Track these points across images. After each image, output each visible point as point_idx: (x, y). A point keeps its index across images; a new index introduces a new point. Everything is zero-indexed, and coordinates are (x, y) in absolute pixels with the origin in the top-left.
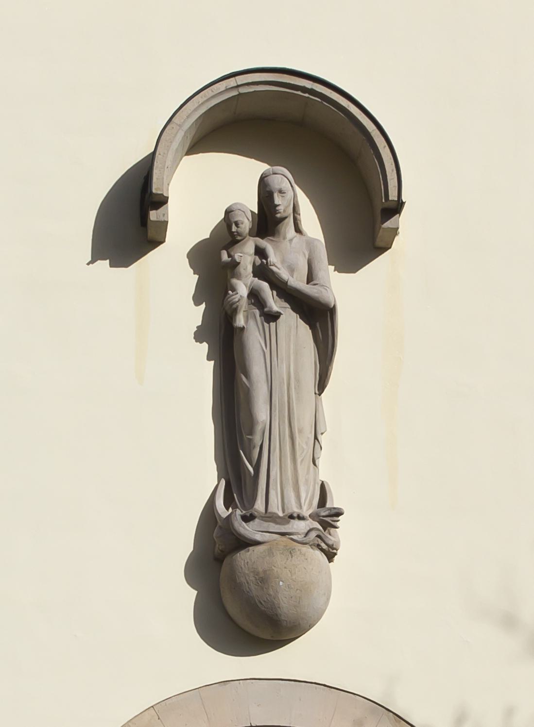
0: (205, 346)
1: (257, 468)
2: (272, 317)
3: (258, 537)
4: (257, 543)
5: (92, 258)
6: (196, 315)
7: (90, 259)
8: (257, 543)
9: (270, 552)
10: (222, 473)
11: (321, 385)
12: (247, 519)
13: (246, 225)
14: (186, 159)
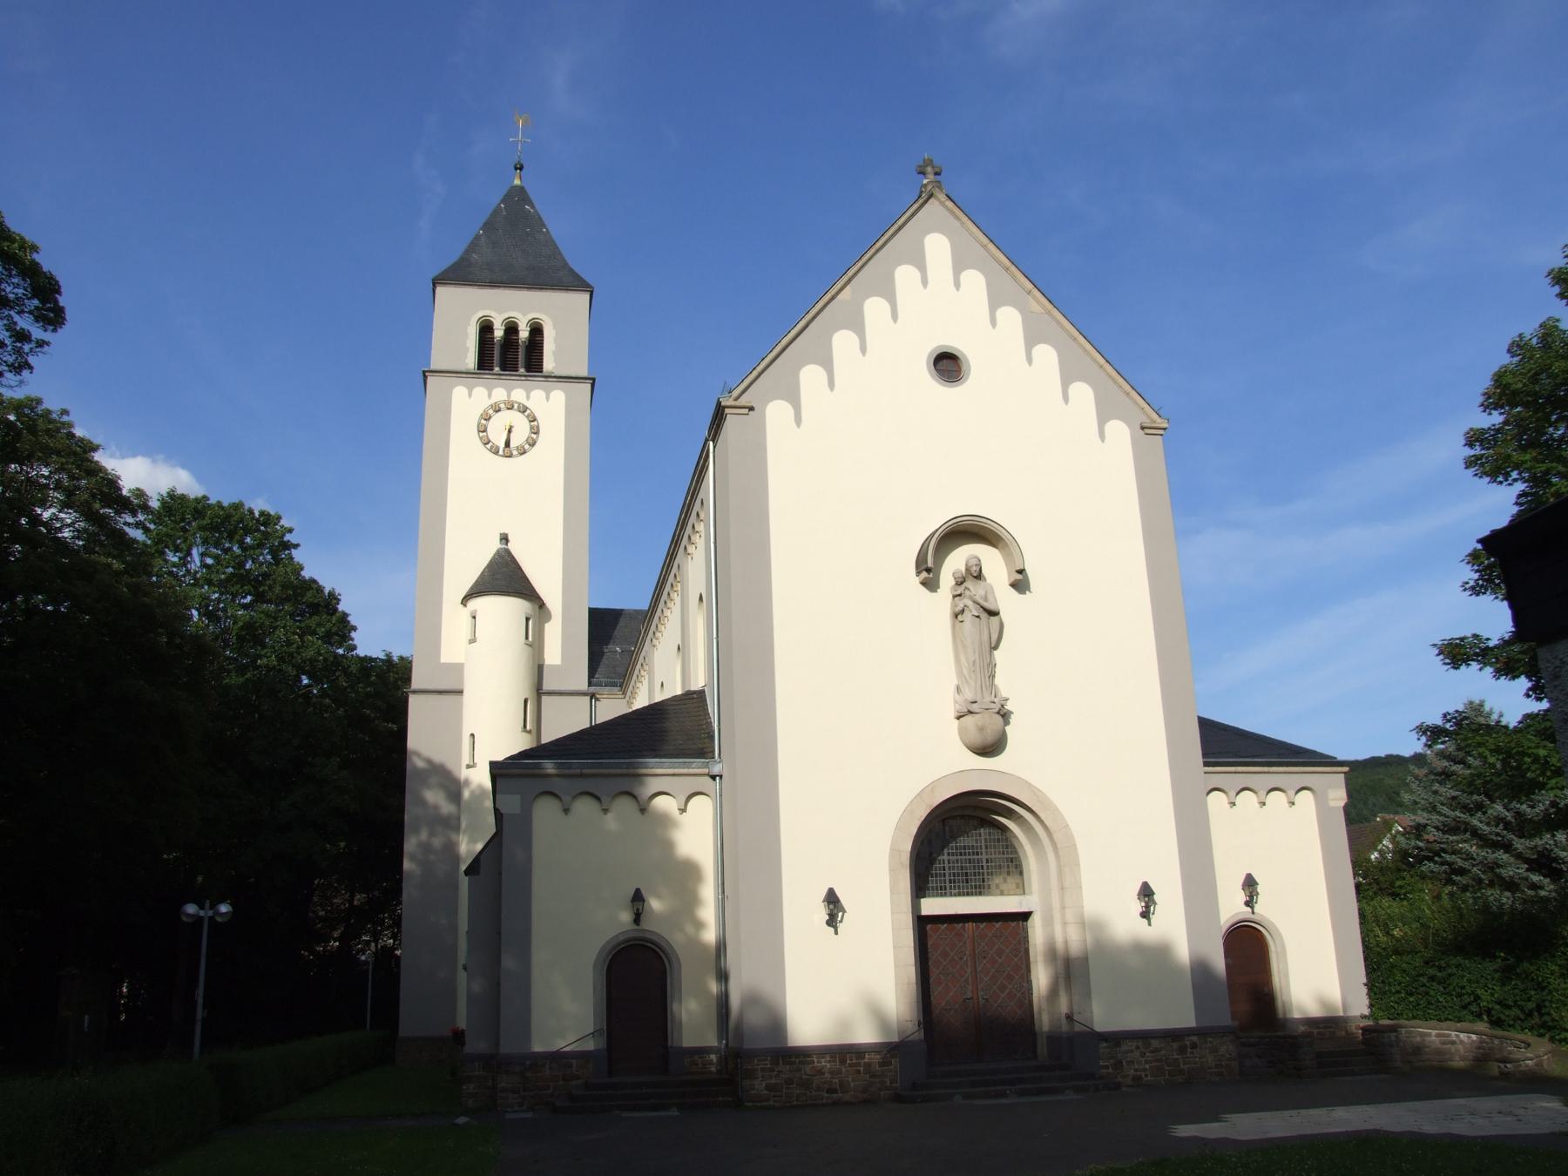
3: (978, 711)
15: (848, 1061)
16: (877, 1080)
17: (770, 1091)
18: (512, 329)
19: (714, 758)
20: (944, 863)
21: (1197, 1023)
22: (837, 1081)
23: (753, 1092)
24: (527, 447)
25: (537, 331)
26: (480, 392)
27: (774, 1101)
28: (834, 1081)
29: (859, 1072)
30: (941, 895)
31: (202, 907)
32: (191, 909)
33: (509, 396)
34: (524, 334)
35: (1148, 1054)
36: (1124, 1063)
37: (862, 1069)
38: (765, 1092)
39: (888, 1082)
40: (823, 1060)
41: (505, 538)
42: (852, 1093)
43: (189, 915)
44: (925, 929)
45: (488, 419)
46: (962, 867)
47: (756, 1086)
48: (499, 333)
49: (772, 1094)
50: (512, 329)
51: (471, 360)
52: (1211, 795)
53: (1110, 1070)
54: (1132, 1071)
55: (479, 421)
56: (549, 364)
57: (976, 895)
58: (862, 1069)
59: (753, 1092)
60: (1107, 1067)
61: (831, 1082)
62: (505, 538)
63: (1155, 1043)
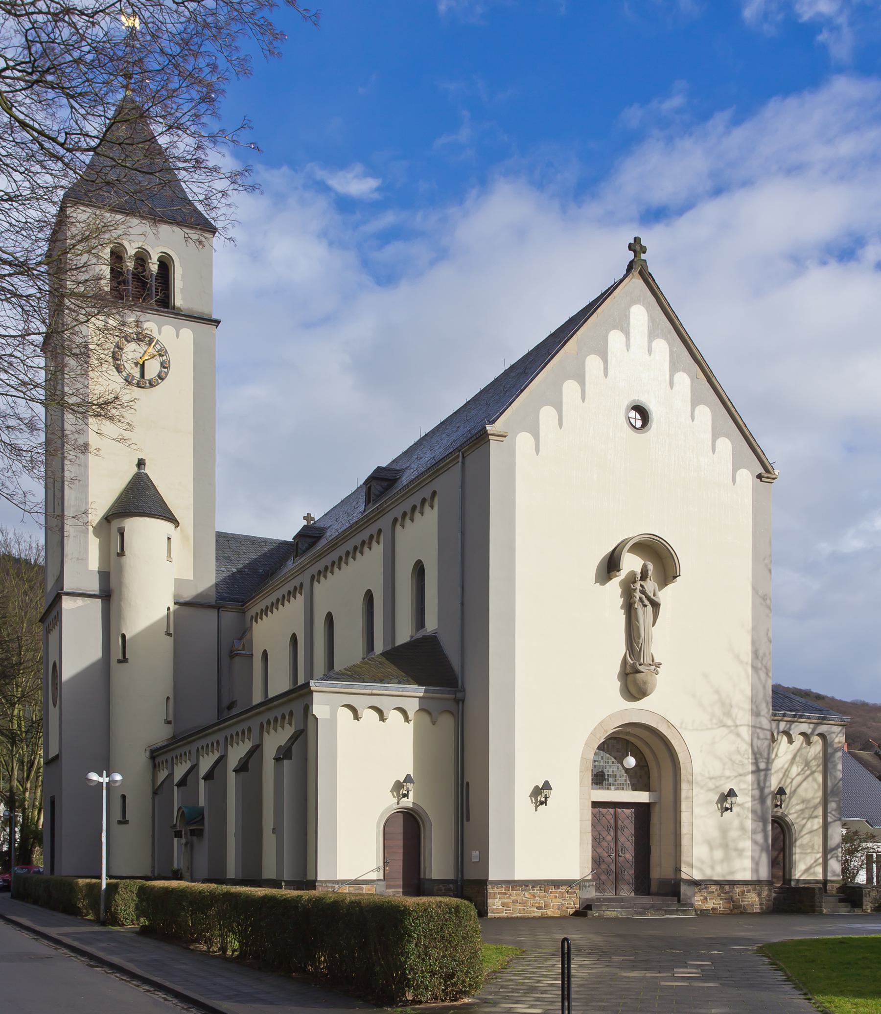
0: (623, 611)
1: (640, 649)
2: (645, 606)
3: (643, 671)
4: (643, 672)
5: (584, 362)
6: (621, 601)
7: (148, 470)
8: (643, 672)
9: (647, 675)
10: (627, 649)
11: (653, 626)
12: (640, 665)
13: (639, 576)
14: (57, 753)
15: (550, 890)
18: (142, 258)
19: (458, 687)
20: (603, 768)
22: (543, 902)
25: (165, 265)
29: (556, 897)
30: (600, 789)
31: (101, 776)
32: (94, 776)
34: (154, 268)
38: (501, 907)
41: (141, 463)
49: (505, 908)
50: (142, 258)
52: (346, 709)
53: (700, 903)
56: (179, 301)
57: (620, 789)
58: (558, 895)
62: (141, 463)
63: (727, 888)
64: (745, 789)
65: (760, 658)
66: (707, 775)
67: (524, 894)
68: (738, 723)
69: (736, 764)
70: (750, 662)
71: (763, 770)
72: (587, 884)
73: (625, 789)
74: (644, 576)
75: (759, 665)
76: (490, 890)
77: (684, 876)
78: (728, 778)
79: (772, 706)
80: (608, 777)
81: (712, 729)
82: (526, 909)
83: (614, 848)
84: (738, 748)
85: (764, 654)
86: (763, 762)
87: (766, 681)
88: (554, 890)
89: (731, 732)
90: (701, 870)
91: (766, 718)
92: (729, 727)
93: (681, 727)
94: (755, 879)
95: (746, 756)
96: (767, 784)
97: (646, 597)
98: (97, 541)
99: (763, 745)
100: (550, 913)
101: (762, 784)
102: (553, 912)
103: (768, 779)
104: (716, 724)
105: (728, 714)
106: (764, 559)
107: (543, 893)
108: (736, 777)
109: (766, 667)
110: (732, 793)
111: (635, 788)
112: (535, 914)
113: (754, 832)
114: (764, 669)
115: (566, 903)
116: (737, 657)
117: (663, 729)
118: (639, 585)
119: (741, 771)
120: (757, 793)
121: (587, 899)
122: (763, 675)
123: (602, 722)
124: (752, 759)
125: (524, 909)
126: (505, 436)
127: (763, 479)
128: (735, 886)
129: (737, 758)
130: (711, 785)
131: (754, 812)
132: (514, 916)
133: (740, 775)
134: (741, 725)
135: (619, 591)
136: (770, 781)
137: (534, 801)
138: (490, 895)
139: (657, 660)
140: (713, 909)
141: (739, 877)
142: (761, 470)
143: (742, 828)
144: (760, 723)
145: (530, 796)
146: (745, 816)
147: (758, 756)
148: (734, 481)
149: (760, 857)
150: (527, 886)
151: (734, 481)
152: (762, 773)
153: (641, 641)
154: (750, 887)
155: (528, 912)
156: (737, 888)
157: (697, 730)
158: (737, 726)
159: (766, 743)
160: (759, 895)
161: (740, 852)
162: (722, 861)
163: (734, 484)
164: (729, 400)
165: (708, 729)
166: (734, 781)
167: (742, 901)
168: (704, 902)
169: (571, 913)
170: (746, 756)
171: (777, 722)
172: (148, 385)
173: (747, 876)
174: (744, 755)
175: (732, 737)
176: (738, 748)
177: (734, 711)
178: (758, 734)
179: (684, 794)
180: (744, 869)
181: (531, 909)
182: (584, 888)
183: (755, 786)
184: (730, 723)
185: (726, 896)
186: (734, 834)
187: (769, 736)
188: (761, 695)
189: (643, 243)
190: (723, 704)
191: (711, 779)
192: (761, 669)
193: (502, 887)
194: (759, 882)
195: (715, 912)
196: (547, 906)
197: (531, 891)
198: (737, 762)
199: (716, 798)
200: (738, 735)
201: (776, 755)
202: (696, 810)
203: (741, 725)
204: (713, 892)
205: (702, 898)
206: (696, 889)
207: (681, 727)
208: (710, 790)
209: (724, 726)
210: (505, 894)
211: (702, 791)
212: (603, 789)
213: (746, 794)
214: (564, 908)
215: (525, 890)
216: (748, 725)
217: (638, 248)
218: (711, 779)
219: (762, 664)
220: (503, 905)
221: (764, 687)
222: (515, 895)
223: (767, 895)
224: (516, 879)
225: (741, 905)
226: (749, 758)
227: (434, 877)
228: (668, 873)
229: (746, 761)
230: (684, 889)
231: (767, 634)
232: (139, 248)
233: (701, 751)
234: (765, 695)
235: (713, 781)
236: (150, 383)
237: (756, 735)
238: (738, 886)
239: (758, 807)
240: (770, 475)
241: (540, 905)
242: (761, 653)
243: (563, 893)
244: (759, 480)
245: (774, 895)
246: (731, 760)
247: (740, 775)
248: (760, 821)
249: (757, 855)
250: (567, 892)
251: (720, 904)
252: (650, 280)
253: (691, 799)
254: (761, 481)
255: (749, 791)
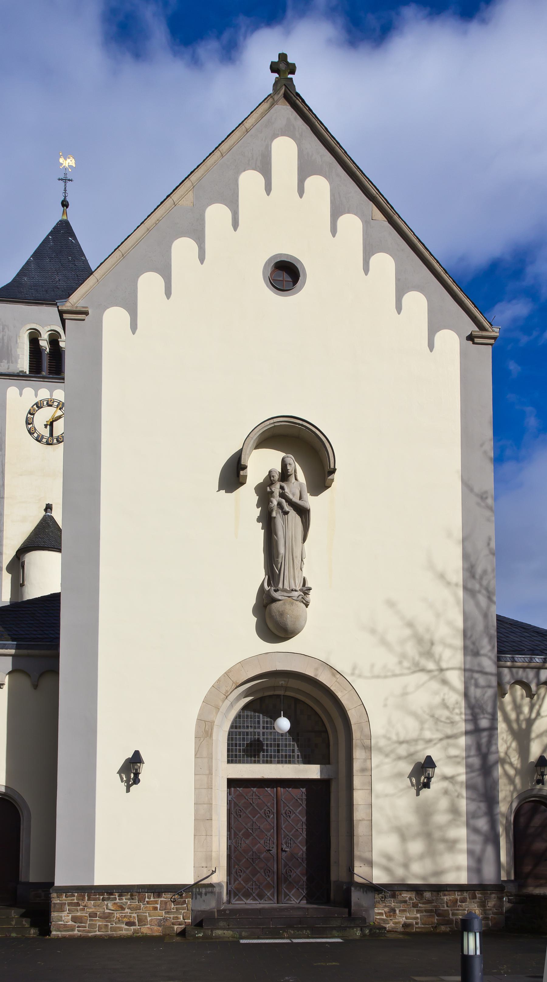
0: (261, 524)
2: (286, 513)
3: (280, 598)
4: (280, 600)
5: (204, 212)
6: (257, 512)
8: (280, 600)
11: (304, 540)
12: (276, 591)
15: (147, 900)
16: (172, 916)
17: (75, 922)
20: (259, 735)
21: (468, 882)
23: (60, 923)
24: (36, 435)
26: (29, 392)
27: (78, 931)
28: (133, 915)
29: (156, 909)
30: (255, 762)
33: (51, 395)
35: (419, 905)
36: (397, 912)
37: (158, 906)
38: (71, 923)
39: (182, 918)
40: (124, 898)
42: (149, 926)
43: (368, 933)
44: (121, 775)
45: (39, 408)
46: (244, 738)
47: (63, 918)
48: (44, 344)
49: (77, 925)
51: (24, 364)
53: (384, 917)
54: (404, 918)
55: (34, 405)
58: (158, 906)
59: (60, 923)
60: (381, 914)
61: (131, 917)
63: (427, 895)
64: (456, 757)
65: (477, 577)
66: (394, 738)
67: (107, 905)
68: (444, 665)
69: (441, 721)
70: (461, 583)
71: (484, 730)
72: (204, 891)
73: (261, 761)
74: (285, 476)
75: (477, 587)
76: (55, 900)
77: (357, 879)
78: (429, 741)
79: (498, 642)
80: (267, 746)
81: (401, 675)
82: (110, 926)
83: (275, 841)
84: (443, 700)
85: (485, 572)
86: (484, 718)
87: (488, 608)
88: (152, 899)
89: (433, 678)
90: (387, 870)
91: (490, 658)
92: (430, 671)
93: (353, 674)
94: (475, 882)
95: (457, 711)
96: (493, 748)
97: (287, 501)
98: (10, 576)
99: (484, 695)
100: (145, 930)
101: (484, 749)
102: (151, 929)
103: (494, 742)
104: (409, 668)
105: (429, 654)
106: (482, 445)
107: (136, 903)
108: (441, 740)
109: (487, 589)
110: (429, 763)
111: (307, 760)
112: (124, 932)
113: (471, 816)
114: (484, 592)
115: (172, 916)
116: (442, 576)
117: (324, 678)
118: (279, 487)
119: (449, 731)
120: (476, 761)
121: (203, 912)
122: (482, 600)
123: (230, 671)
124: (466, 714)
125: (107, 926)
126: (86, 313)
127: (477, 340)
128: (441, 894)
129: (444, 714)
130: (402, 750)
131: (469, 786)
132: (90, 934)
133: (448, 737)
134: (447, 669)
135: (255, 498)
136: (496, 744)
137: (125, 779)
138: (55, 906)
139: (309, 584)
140: (405, 925)
141: (450, 879)
142: (472, 328)
143: (454, 810)
144: (479, 665)
145: (120, 772)
146: (456, 794)
147: (477, 710)
148: (431, 346)
149: (483, 851)
150: (111, 894)
151: (431, 346)
152: (485, 734)
153: (280, 560)
154: (466, 894)
155: (113, 929)
156: (445, 895)
157: (378, 677)
158: (441, 670)
159: (490, 692)
160: (483, 905)
161: (451, 845)
162: (422, 857)
163: (431, 350)
164: (420, 241)
165: (395, 675)
166: (439, 745)
167: (453, 914)
168: (390, 916)
169: (179, 930)
170: (457, 711)
171: (535, 670)
172: (55, 441)
173: (462, 878)
174: (454, 709)
175: (435, 685)
176: (443, 700)
177: (438, 649)
178: (476, 680)
179: (357, 766)
180: (458, 868)
181: (118, 925)
182: (198, 897)
183: (473, 752)
184: (431, 666)
185: (428, 907)
186: (441, 818)
187: (494, 681)
188: (480, 626)
189: (290, 60)
190: (420, 640)
191: (401, 743)
192: (479, 592)
193: (74, 896)
194: (482, 887)
195: (408, 930)
196: (142, 921)
197: (118, 901)
198: (443, 719)
199: (408, 768)
200: (445, 682)
201: (538, 714)
202: (378, 787)
203: (447, 669)
204: (405, 902)
205: (386, 909)
206: (378, 897)
207: (353, 674)
208: (399, 758)
209: (423, 670)
210: (78, 904)
211: (387, 760)
212: (259, 762)
213: (459, 763)
214: (168, 924)
215: (108, 899)
216: (460, 669)
217: (282, 66)
218: (401, 743)
219: (481, 585)
220: (74, 919)
221: (486, 616)
222: (91, 905)
223: (494, 906)
224: (95, 884)
225: (452, 920)
226: (461, 714)
227: (33, 879)
228: (343, 877)
229: (457, 718)
230: (356, 896)
231: (489, 544)
232: (49, 331)
233: (385, 706)
234: (487, 627)
235: (404, 746)
236: (57, 440)
237: (473, 681)
238: (446, 892)
239: (479, 780)
240: (485, 334)
241: (132, 919)
242: (479, 570)
243: (166, 903)
244: (471, 342)
245: (507, 906)
246: (433, 716)
247: (448, 737)
248: (481, 801)
249: (478, 848)
250: (173, 902)
251: (416, 918)
252: (299, 102)
253: (367, 770)
254: (474, 343)
255: (463, 758)
